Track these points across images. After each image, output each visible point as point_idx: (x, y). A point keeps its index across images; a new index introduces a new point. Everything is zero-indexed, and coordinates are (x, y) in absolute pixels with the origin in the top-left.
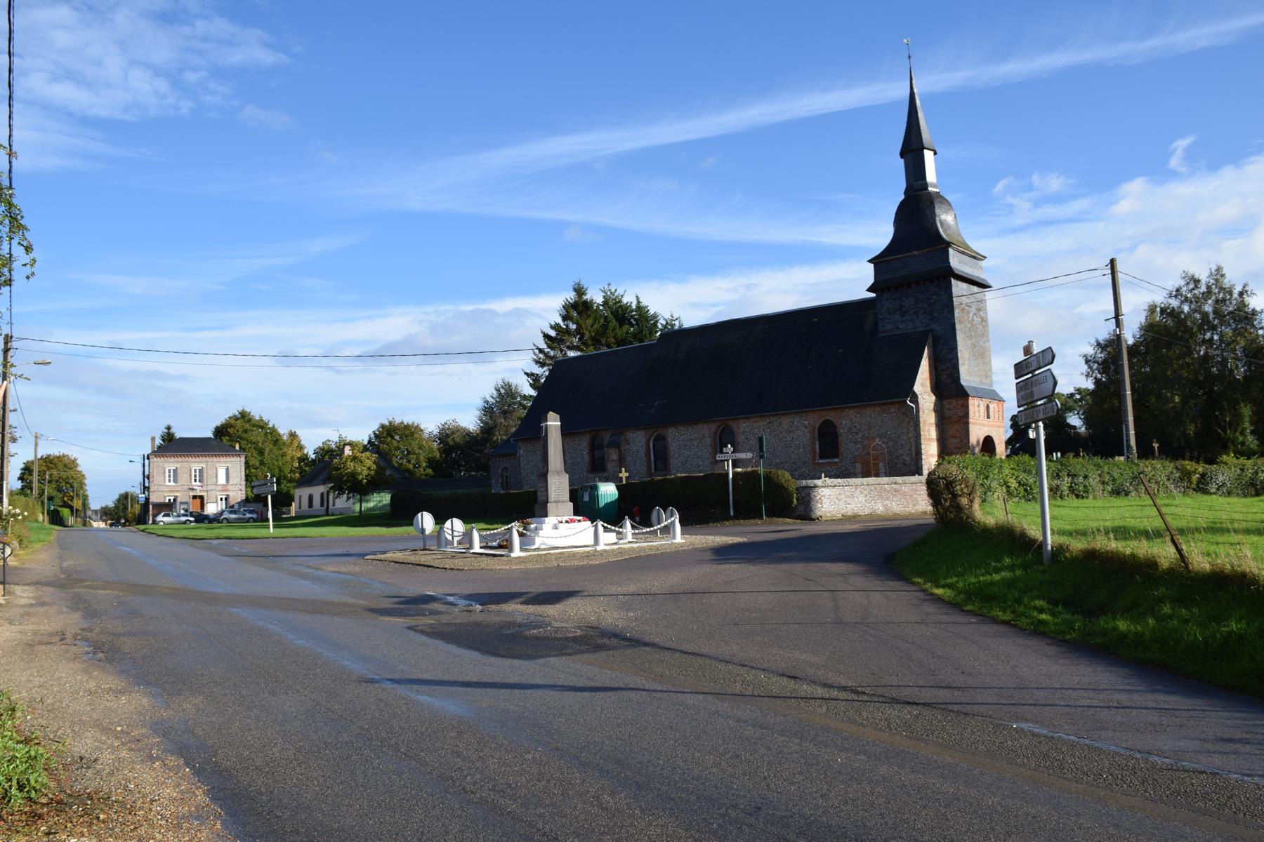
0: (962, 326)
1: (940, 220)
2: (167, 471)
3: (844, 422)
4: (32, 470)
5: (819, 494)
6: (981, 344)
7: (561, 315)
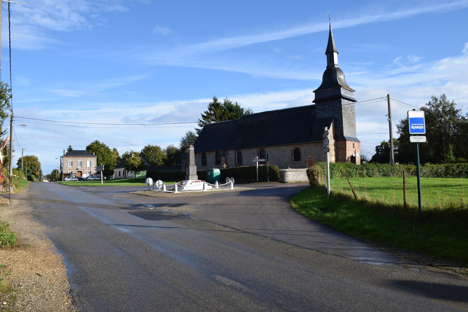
0: (345, 115)
1: (338, 78)
2: (69, 162)
3: (302, 149)
4: (21, 161)
5: (287, 174)
6: (352, 122)
7: (208, 108)
